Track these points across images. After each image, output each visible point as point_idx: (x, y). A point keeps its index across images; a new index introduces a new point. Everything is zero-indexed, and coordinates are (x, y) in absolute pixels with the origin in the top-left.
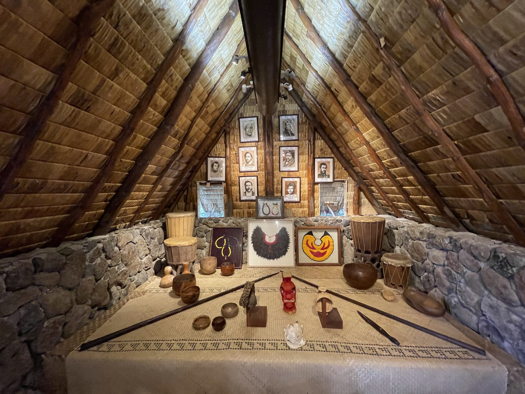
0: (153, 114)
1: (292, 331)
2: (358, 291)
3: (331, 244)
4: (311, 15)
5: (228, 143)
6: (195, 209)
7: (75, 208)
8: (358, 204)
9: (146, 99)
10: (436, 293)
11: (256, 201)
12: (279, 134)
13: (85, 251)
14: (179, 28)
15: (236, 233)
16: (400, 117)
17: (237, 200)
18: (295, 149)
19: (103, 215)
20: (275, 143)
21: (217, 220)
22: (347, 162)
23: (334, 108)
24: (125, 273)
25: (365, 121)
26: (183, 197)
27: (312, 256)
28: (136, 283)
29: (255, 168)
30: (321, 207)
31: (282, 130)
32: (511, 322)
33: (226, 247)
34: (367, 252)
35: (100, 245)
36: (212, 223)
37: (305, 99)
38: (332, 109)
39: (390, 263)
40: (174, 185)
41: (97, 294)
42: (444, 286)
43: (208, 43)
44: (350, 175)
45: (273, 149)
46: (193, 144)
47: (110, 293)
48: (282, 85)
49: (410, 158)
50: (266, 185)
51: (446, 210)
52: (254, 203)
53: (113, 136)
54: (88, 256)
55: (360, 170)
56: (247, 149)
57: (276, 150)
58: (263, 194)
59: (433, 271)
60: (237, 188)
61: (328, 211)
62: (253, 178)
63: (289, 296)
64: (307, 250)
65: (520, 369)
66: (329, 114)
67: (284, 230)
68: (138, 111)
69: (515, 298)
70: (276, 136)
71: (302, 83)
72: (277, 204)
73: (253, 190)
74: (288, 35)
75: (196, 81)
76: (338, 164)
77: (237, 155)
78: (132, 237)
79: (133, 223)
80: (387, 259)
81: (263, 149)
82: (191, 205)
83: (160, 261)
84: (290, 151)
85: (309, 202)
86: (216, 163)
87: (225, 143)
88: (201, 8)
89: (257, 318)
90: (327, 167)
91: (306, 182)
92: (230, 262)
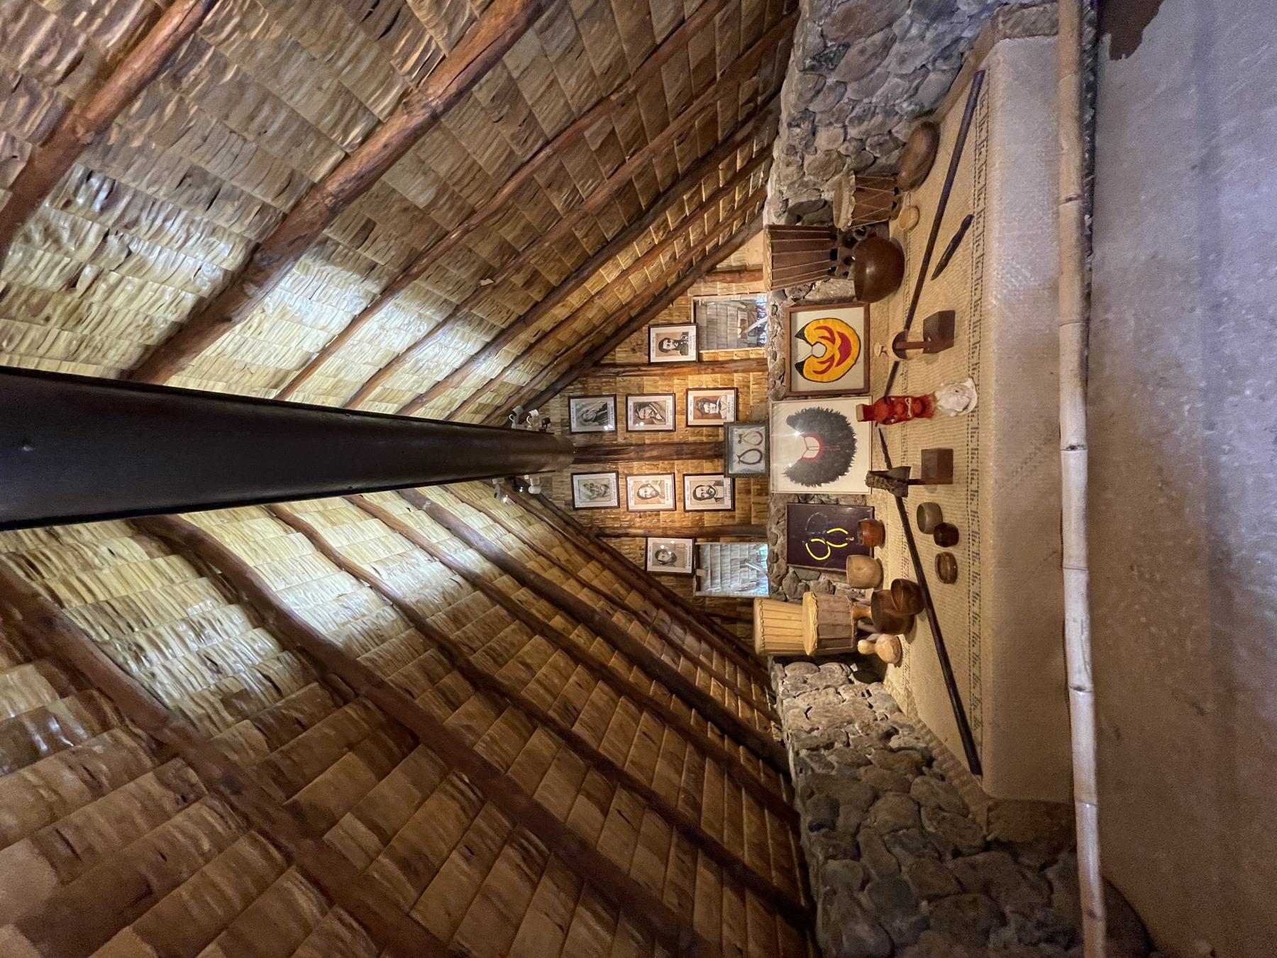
0: (578, 635)
1: (947, 402)
2: (906, 274)
3: (822, 323)
4: (431, 383)
5: (620, 532)
6: (749, 602)
7: (731, 778)
8: (741, 272)
9: (557, 640)
10: (901, 131)
11: (733, 478)
12: (602, 433)
13: (810, 772)
14: (458, 578)
15: (800, 515)
16: (586, 236)
17: (733, 517)
18: (632, 401)
19: (750, 749)
20: (620, 440)
21: (773, 558)
22: (657, 302)
23: (564, 335)
24: (866, 727)
25: (591, 286)
26: (727, 627)
27: (849, 361)
28: (892, 712)
29: (668, 480)
30: (750, 345)
31: (593, 427)
32: (922, 37)
33: (828, 537)
34: (833, 255)
35: (803, 753)
36: (779, 567)
37: (542, 387)
38: (563, 339)
39: (850, 216)
40: (700, 637)
41: (897, 765)
42: (883, 124)
43: (469, 544)
44: (683, 292)
45: (631, 445)
46: (622, 591)
47: (900, 749)
48: (513, 426)
49: (649, 207)
50: (702, 458)
51: (739, 136)
52: (738, 481)
53: (613, 695)
54: (819, 771)
55: (674, 276)
56: (631, 493)
57: (634, 439)
58: (719, 465)
59: (861, 140)
60: (706, 516)
61: (760, 330)
62: (687, 483)
63: (899, 409)
64: (836, 371)
65: (1001, 19)
66: (570, 343)
67: (792, 421)
68: (576, 655)
69: (878, 37)
70: (607, 440)
71: (518, 392)
72: (740, 436)
73: (712, 484)
74: (451, 415)
75: (525, 567)
76: (662, 317)
77: (643, 514)
78: (796, 710)
79: (773, 716)
80: (844, 220)
81: (630, 464)
82: (741, 610)
83: (855, 674)
84: (636, 411)
85: (736, 371)
86: (657, 555)
87: (618, 536)
88: (432, 545)
89: (941, 466)
90: (668, 338)
91: (696, 377)
92: (863, 534)
